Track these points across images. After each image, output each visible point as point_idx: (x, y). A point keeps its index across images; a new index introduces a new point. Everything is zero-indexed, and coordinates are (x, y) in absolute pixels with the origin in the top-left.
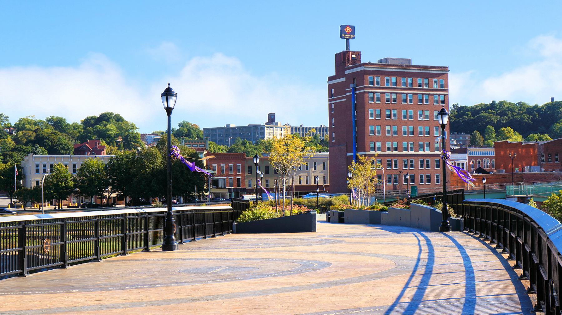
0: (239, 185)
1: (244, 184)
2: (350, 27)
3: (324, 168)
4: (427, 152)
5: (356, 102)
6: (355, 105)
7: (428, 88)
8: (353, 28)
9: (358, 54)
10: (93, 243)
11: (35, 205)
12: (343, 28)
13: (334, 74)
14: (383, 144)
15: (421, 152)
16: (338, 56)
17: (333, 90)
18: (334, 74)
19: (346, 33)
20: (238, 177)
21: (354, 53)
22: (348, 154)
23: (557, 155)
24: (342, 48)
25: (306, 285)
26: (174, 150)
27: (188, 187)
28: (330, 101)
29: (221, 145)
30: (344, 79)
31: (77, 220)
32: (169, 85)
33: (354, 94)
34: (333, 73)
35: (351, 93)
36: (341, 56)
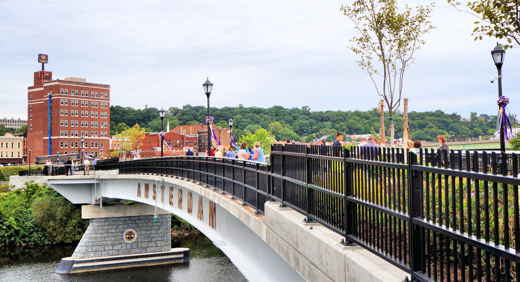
0: (12, 156)
3: (19, 147)
4: (96, 138)
7: (97, 98)
8: (47, 56)
9: (50, 73)
10: (343, 166)
11: (435, 152)
12: (40, 56)
14: (69, 132)
15: (92, 137)
16: (36, 74)
19: (42, 59)
21: (47, 73)
22: (44, 138)
23: (170, 141)
24: (39, 69)
28: (29, 102)
30: (42, 89)
31: (367, 158)
33: (50, 99)
34: (33, 85)
35: (48, 99)
36: (38, 74)
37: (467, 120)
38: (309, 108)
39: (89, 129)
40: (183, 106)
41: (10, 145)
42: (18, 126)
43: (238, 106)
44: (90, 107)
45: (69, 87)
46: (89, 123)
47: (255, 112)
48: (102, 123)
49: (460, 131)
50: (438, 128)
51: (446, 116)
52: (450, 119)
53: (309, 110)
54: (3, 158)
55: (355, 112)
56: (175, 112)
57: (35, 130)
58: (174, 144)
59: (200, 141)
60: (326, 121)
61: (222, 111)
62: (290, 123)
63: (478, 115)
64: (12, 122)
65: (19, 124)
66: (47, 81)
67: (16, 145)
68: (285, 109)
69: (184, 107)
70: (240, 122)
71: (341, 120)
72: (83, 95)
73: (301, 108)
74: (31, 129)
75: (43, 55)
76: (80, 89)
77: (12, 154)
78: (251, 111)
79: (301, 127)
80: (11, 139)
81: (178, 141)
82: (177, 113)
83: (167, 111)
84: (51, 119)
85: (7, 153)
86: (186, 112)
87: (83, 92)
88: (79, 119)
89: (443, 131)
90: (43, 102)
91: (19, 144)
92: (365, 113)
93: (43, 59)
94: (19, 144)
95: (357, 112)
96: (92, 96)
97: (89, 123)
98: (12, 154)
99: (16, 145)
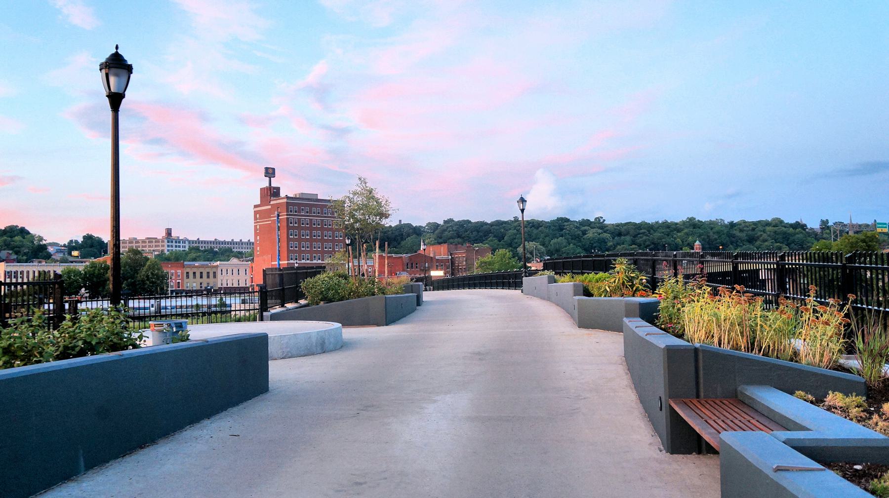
1: (182, 286)
2: (272, 168)
5: (279, 225)
6: (279, 227)
8: (274, 169)
9: (278, 189)
12: (267, 169)
13: (259, 203)
14: (300, 256)
17: (258, 215)
18: (259, 203)
19: (269, 173)
20: (178, 281)
21: (274, 188)
25: (50, 275)
26: (211, 247)
27: (682, 472)
28: (255, 223)
29: (55, 274)
30: (269, 207)
32: (117, 47)
33: (278, 218)
34: (259, 202)
36: (265, 190)
37: (815, 230)
38: (603, 219)
39: (311, 252)
40: (444, 221)
41: (235, 271)
42: (248, 249)
43: (513, 219)
44: (322, 227)
45: (299, 205)
46: (322, 245)
47: (533, 226)
48: (337, 245)
49: (806, 245)
50: (775, 242)
51: (786, 225)
52: (791, 229)
53: (604, 222)
54: (229, 286)
55: (664, 223)
56: (434, 227)
57: (263, 253)
58: (422, 268)
59: (453, 263)
60: (625, 235)
61: (492, 226)
62: (577, 239)
63: (830, 224)
64: (241, 244)
65: (249, 246)
66: (275, 198)
67: (242, 272)
68: (572, 221)
69: (445, 222)
70: (515, 239)
71: (643, 233)
72: (314, 213)
73: (592, 220)
74: (258, 253)
75: (270, 168)
76: (311, 206)
77: (239, 282)
78: (529, 224)
79: (592, 244)
80: (237, 264)
81: (427, 264)
82: (437, 229)
83: (424, 227)
84: (279, 242)
85: (232, 280)
86: (447, 227)
87: (314, 209)
88: (311, 241)
89: (781, 245)
90: (270, 222)
91: (246, 270)
92: (676, 224)
93: (270, 173)
94: (246, 270)
95: (665, 222)
96: (325, 214)
97: (322, 245)
98: (239, 282)
99: (242, 272)
